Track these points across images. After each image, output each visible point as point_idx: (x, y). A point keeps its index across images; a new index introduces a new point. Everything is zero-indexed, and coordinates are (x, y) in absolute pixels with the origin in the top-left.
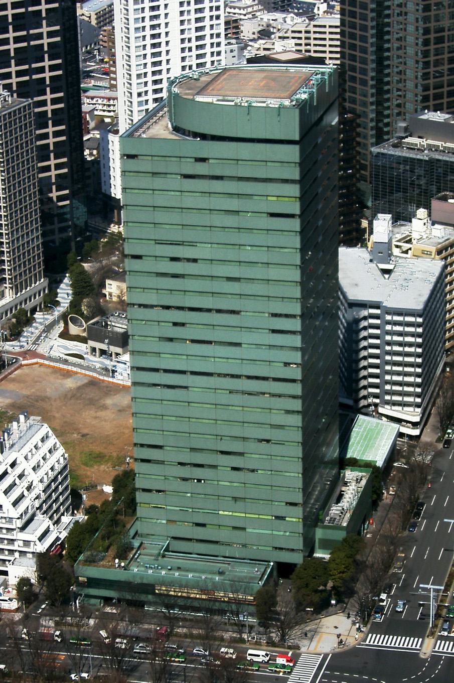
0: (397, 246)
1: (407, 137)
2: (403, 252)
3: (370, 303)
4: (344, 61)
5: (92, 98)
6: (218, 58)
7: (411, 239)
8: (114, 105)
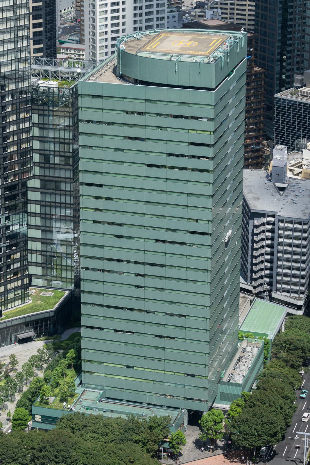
0: (291, 170)
1: (302, 87)
2: (296, 175)
3: (268, 213)
4: (257, 27)
5: (67, 49)
6: (162, 22)
7: (302, 165)
8: (83, 55)
